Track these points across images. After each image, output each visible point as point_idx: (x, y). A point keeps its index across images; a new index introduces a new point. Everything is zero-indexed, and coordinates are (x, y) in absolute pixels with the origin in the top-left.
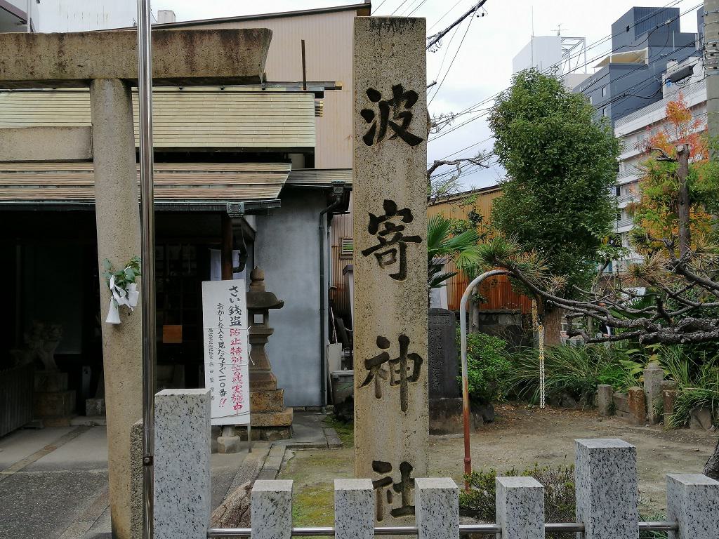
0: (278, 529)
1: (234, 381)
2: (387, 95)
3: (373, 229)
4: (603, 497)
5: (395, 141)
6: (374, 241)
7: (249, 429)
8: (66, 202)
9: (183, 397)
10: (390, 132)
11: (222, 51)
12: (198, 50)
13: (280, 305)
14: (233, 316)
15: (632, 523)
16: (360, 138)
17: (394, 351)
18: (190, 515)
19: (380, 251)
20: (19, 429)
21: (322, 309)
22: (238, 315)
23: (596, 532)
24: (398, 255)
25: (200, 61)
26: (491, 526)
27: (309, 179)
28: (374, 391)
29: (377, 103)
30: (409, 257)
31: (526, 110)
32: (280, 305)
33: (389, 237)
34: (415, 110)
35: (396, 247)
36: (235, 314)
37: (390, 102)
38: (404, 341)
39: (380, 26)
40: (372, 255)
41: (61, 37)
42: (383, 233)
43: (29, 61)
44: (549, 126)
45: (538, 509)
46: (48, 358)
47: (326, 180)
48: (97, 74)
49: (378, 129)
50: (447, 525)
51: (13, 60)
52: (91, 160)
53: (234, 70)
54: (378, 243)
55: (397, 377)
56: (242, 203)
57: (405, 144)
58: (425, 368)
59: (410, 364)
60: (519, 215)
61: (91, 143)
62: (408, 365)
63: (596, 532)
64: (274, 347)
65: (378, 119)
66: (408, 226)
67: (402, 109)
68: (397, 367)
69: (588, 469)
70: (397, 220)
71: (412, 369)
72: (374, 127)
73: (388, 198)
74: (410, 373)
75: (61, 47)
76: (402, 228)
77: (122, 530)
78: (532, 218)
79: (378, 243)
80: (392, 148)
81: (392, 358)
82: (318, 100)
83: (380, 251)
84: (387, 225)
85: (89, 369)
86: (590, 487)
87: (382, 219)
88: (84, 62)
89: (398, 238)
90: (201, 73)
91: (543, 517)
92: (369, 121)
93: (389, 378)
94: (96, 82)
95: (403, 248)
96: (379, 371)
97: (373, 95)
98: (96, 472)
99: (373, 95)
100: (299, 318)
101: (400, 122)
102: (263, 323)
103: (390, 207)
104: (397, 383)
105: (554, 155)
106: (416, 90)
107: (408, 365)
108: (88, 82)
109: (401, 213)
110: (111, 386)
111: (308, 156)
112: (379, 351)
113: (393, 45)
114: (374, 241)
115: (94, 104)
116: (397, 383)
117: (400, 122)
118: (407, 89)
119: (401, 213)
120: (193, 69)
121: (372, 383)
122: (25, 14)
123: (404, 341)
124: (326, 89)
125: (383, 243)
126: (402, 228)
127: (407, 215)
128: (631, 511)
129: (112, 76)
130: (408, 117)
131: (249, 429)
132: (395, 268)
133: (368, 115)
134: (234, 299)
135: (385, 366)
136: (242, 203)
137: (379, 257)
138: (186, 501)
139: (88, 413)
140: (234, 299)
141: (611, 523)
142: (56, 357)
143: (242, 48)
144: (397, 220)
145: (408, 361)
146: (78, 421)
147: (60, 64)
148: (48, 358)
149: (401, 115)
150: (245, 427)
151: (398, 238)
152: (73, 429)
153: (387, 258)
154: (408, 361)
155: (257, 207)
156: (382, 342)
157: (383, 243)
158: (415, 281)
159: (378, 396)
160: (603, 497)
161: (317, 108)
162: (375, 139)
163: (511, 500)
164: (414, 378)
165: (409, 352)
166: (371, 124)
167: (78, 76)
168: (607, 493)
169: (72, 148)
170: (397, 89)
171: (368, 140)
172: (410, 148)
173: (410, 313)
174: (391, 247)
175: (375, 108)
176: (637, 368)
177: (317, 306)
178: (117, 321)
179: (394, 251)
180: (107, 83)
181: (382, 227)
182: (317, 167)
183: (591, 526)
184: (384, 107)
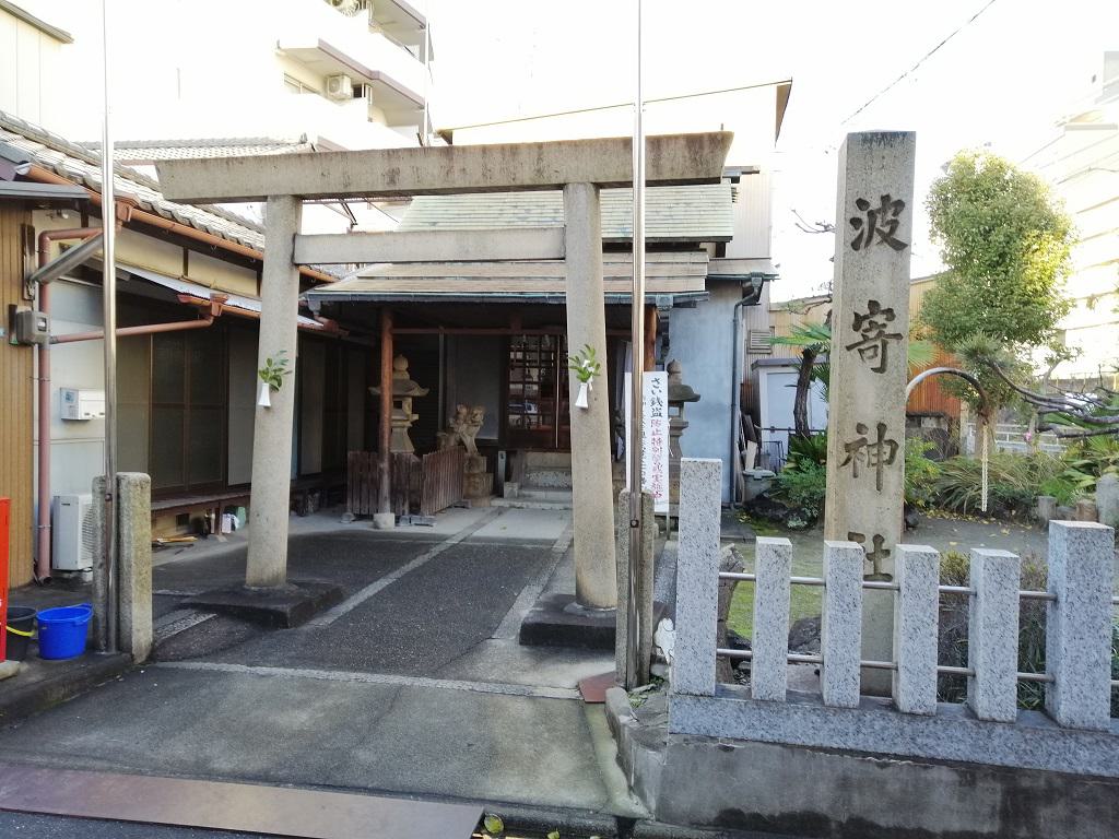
0: (780, 576)
1: (654, 470)
2: (875, 204)
3: (856, 327)
4: (1078, 571)
5: (882, 247)
6: (858, 337)
7: (668, 518)
8: (505, 295)
9: (703, 463)
10: (877, 238)
11: (687, 154)
12: (665, 154)
13: (696, 399)
14: (654, 407)
15: (1106, 596)
16: (849, 244)
17: (872, 437)
18: (707, 559)
19: (862, 347)
20: (450, 507)
21: (733, 405)
22: (659, 407)
23: (1069, 600)
24: (880, 350)
25: (666, 163)
26: (963, 588)
27: (727, 269)
28: (851, 471)
29: (866, 212)
30: (890, 353)
31: (968, 193)
32: (696, 399)
33: (872, 334)
34: (902, 217)
35: (879, 343)
36: (657, 404)
37: (879, 211)
38: (881, 428)
39: (871, 141)
40: (856, 349)
41: (540, 146)
42: (866, 331)
43: (512, 169)
44: (997, 211)
45: (1013, 577)
46: (470, 441)
47: (741, 270)
48: (571, 179)
49: (865, 236)
50: (928, 583)
51: (498, 167)
52: (563, 259)
53: (698, 174)
54: (861, 339)
55: (874, 460)
56: (671, 296)
57: (891, 249)
58: (900, 454)
59: (887, 449)
60: (955, 309)
61: (563, 242)
62: (885, 450)
63: (1069, 600)
64: (686, 438)
65: (865, 226)
66: (889, 324)
67: (890, 217)
68: (875, 451)
69: (1065, 545)
70: (880, 319)
71: (888, 454)
72: (862, 233)
73: (872, 298)
74: (886, 457)
75: (539, 155)
76: (884, 325)
77: (766, 526)
78: (968, 314)
79: (861, 339)
80: (879, 253)
81: (870, 443)
82: (734, 185)
83: (862, 347)
84: (871, 323)
85: (504, 453)
86: (1065, 562)
87: (866, 317)
88: (557, 170)
89: (880, 334)
90: (667, 176)
91: (1018, 583)
92: (857, 229)
93: (866, 461)
94: (570, 186)
95: (884, 345)
96: (858, 454)
97: (862, 204)
98: (529, 546)
99: (862, 204)
100: (710, 413)
101: (886, 229)
102: (679, 416)
103: (873, 305)
104: (873, 465)
105: (1000, 243)
106: (904, 200)
107: (885, 450)
108: (560, 187)
109: (883, 312)
110: (578, 461)
111: (720, 245)
112: (859, 437)
113: (883, 158)
114: (858, 337)
115: (568, 206)
116: (873, 465)
117: (886, 229)
118: (895, 198)
119: (883, 312)
120: (659, 173)
121: (851, 463)
122: (423, 100)
123: (881, 428)
124: (743, 173)
125: (866, 339)
126: (884, 325)
127: (890, 313)
128: (1105, 585)
129: (585, 180)
130: (894, 224)
131: (668, 518)
132: (877, 363)
133: (855, 222)
134: (656, 391)
135: (863, 450)
136: (671, 296)
137: (861, 351)
138: (704, 547)
139: (505, 495)
140: (656, 391)
141: (1085, 594)
142: (476, 440)
143: (706, 151)
144: (880, 319)
145: (885, 446)
146: (498, 502)
147: (539, 171)
148: (470, 441)
149: (888, 223)
150: (664, 517)
151: (880, 334)
152: (492, 509)
153: (870, 353)
154: (885, 446)
155: (687, 300)
156: (860, 428)
157: (866, 339)
158: (895, 374)
159: (855, 476)
160: (1078, 571)
161: (734, 193)
162: (863, 244)
163: (988, 567)
164: (890, 462)
165: (887, 437)
166: (859, 231)
167: (555, 181)
168: (1082, 567)
169: (543, 246)
170: (885, 199)
171: (855, 245)
172: (895, 252)
173: (889, 404)
174: (873, 344)
175: (864, 216)
176: (1088, 480)
177: (728, 401)
178: (586, 405)
179: (876, 346)
180: (581, 187)
181: (866, 325)
182: (727, 257)
183: (1065, 595)
184: (871, 214)
